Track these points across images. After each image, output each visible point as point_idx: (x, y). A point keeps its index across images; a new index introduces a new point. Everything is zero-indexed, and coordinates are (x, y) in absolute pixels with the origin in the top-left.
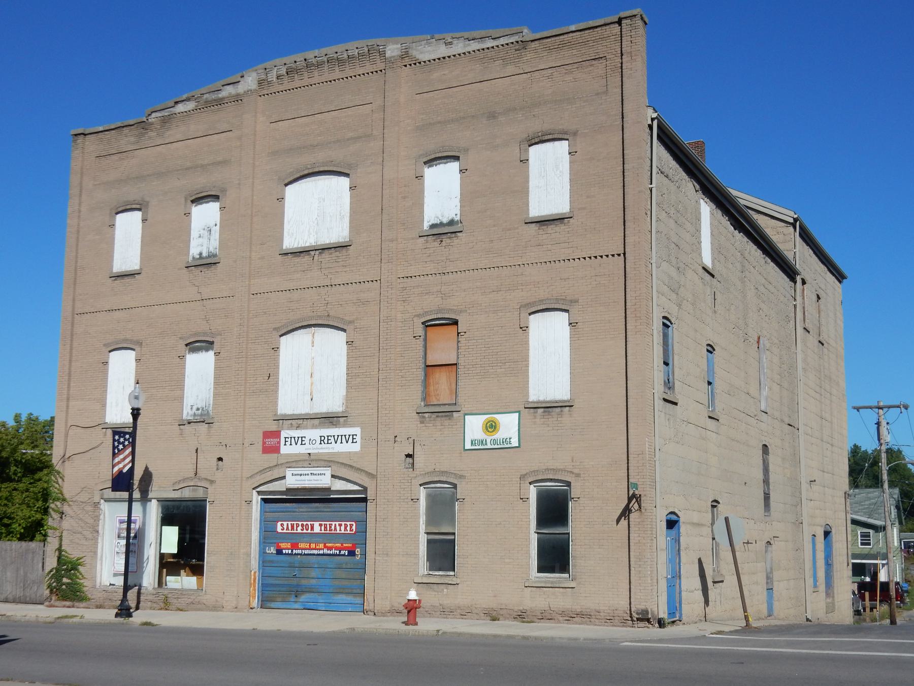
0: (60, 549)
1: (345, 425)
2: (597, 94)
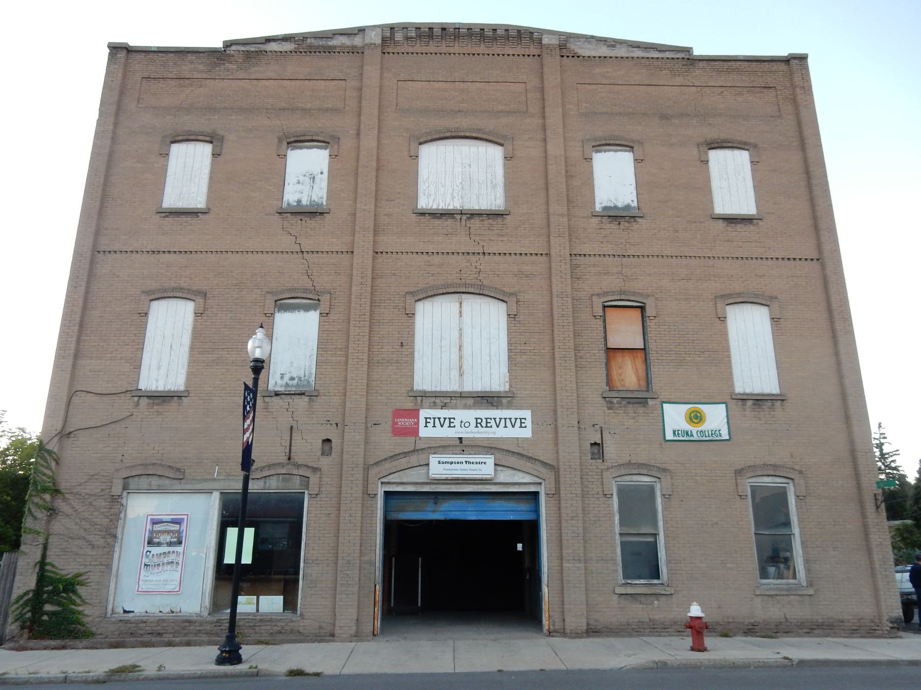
0: (42, 563)
1: (509, 406)
2: (772, 117)
